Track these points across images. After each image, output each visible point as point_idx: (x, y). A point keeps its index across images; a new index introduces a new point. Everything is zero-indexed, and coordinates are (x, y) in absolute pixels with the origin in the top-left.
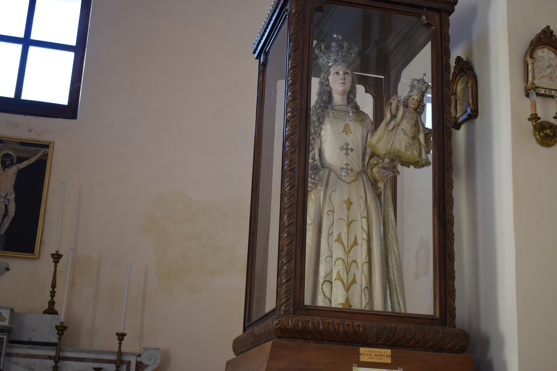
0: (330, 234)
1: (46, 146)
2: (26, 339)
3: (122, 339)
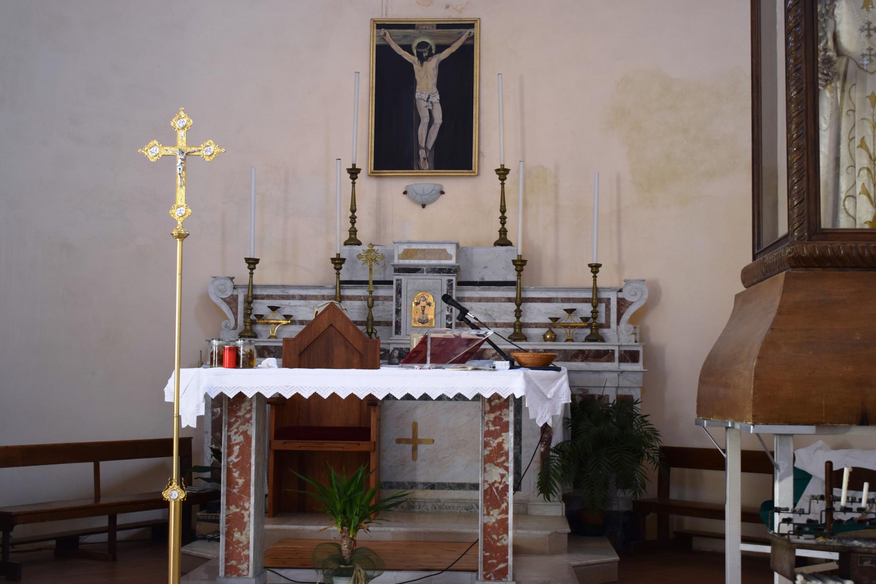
0: (851, 139)
1: (471, 26)
2: (477, 279)
3: (597, 272)
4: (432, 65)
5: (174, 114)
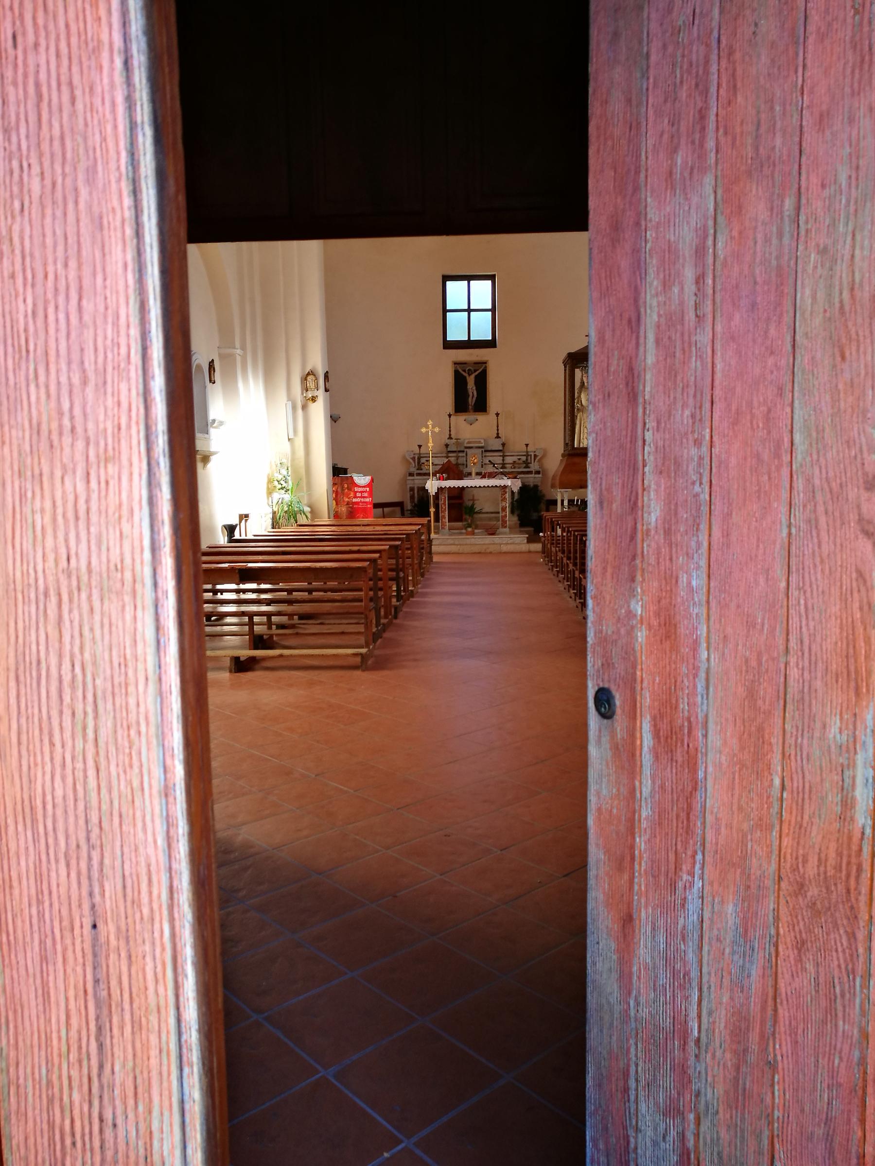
4: (473, 376)
5: (428, 421)
